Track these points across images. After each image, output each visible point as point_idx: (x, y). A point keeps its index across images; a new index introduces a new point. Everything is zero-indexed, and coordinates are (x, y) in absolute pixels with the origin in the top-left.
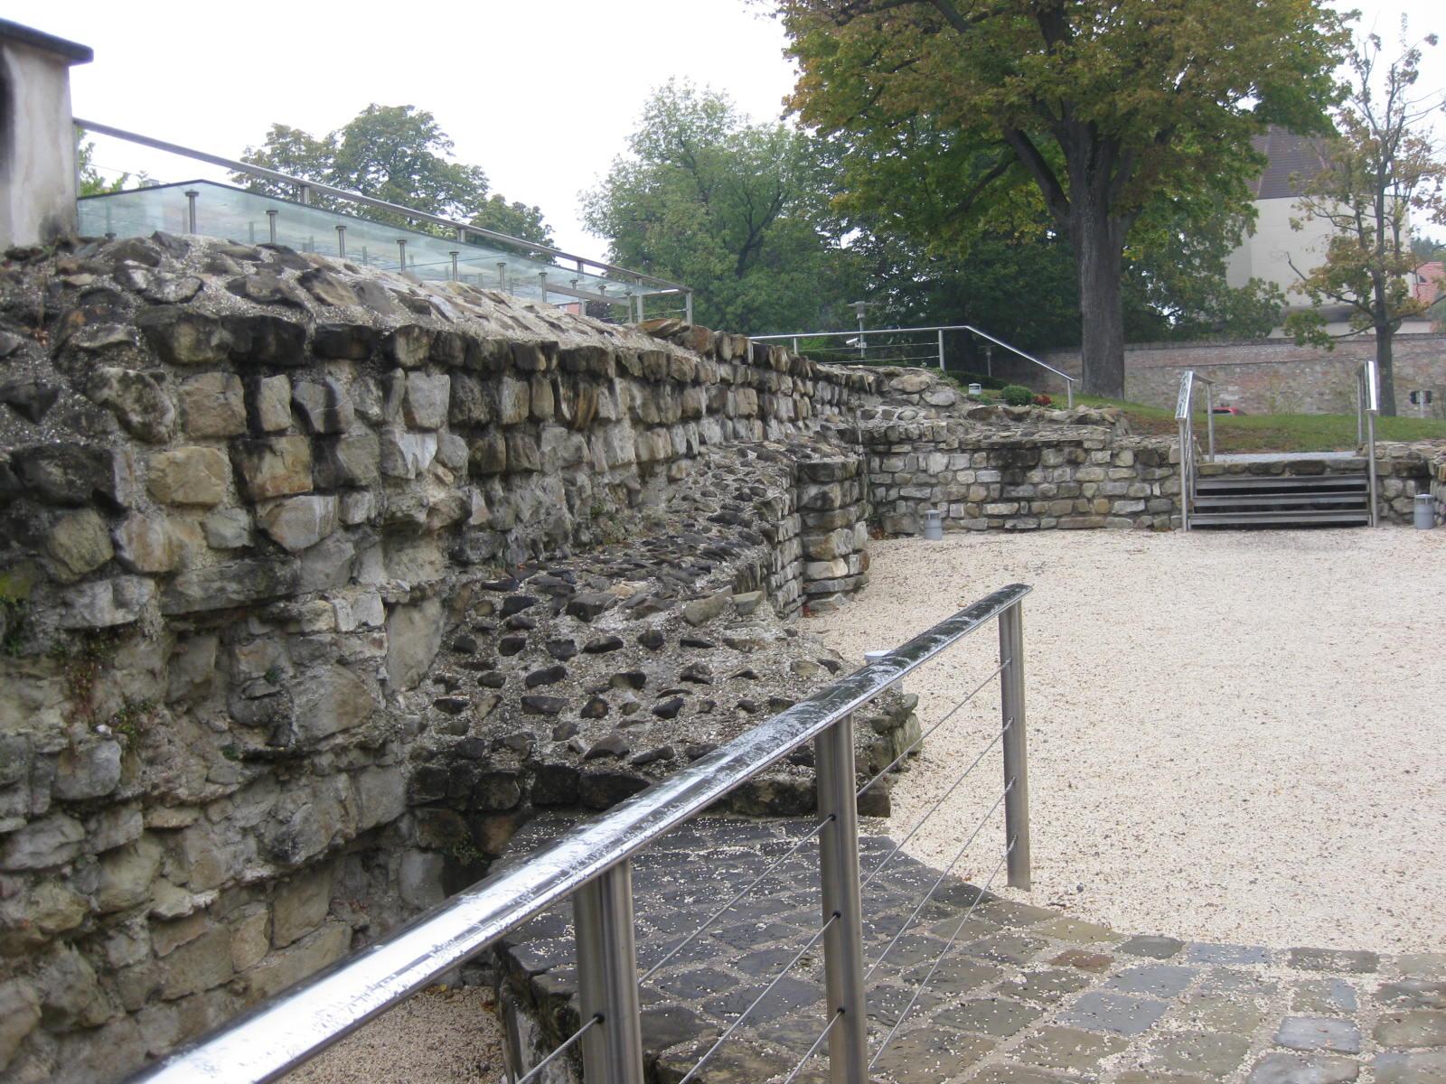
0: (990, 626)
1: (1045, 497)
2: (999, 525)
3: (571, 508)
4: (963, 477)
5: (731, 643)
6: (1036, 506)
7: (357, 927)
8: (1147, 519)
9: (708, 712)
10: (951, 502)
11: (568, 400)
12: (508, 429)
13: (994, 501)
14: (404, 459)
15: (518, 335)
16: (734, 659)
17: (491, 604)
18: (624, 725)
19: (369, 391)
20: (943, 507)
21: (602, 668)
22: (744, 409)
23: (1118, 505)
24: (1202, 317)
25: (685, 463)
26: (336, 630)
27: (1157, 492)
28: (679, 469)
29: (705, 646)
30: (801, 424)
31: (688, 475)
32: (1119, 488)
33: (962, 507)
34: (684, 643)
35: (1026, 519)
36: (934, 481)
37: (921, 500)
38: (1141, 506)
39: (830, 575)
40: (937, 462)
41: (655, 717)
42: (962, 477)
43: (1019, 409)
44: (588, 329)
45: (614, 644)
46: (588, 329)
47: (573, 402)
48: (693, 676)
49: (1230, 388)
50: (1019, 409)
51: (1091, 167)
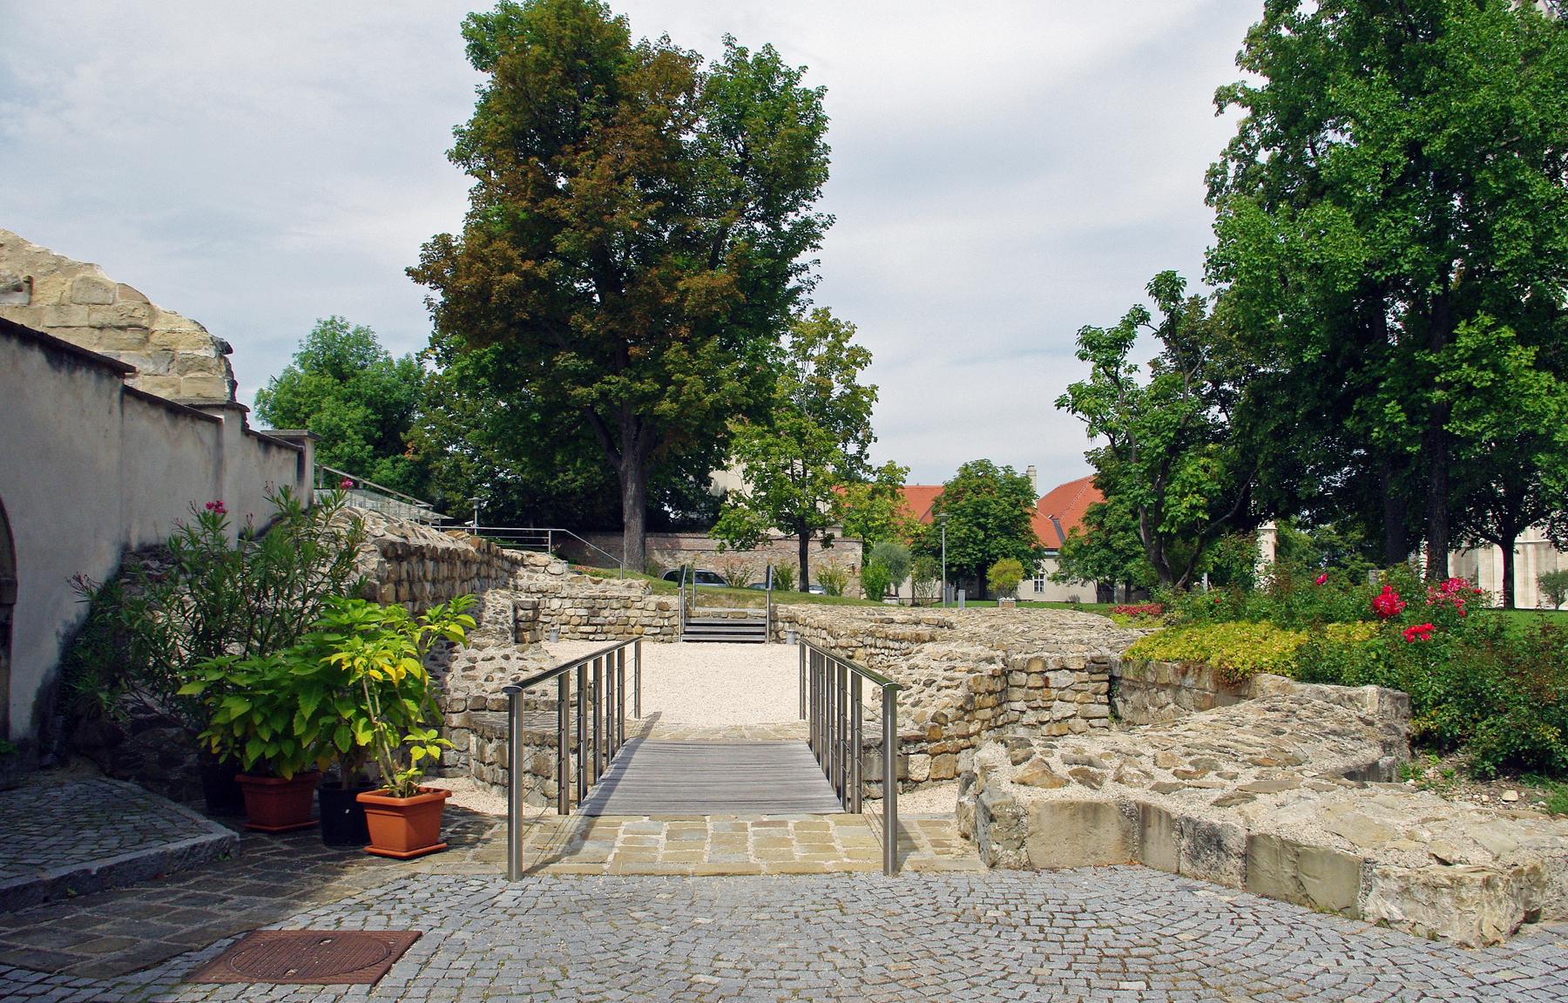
4: (570, 612)
8: (661, 637)
21: (489, 666)
24: (694, 516)
32: (646, 621)
38: (658, 630)
40: (555, 603)
42: (567, 611)
43: (596, 579)
45: (492, 658)
50: (596, 579)
51: (636, 439)
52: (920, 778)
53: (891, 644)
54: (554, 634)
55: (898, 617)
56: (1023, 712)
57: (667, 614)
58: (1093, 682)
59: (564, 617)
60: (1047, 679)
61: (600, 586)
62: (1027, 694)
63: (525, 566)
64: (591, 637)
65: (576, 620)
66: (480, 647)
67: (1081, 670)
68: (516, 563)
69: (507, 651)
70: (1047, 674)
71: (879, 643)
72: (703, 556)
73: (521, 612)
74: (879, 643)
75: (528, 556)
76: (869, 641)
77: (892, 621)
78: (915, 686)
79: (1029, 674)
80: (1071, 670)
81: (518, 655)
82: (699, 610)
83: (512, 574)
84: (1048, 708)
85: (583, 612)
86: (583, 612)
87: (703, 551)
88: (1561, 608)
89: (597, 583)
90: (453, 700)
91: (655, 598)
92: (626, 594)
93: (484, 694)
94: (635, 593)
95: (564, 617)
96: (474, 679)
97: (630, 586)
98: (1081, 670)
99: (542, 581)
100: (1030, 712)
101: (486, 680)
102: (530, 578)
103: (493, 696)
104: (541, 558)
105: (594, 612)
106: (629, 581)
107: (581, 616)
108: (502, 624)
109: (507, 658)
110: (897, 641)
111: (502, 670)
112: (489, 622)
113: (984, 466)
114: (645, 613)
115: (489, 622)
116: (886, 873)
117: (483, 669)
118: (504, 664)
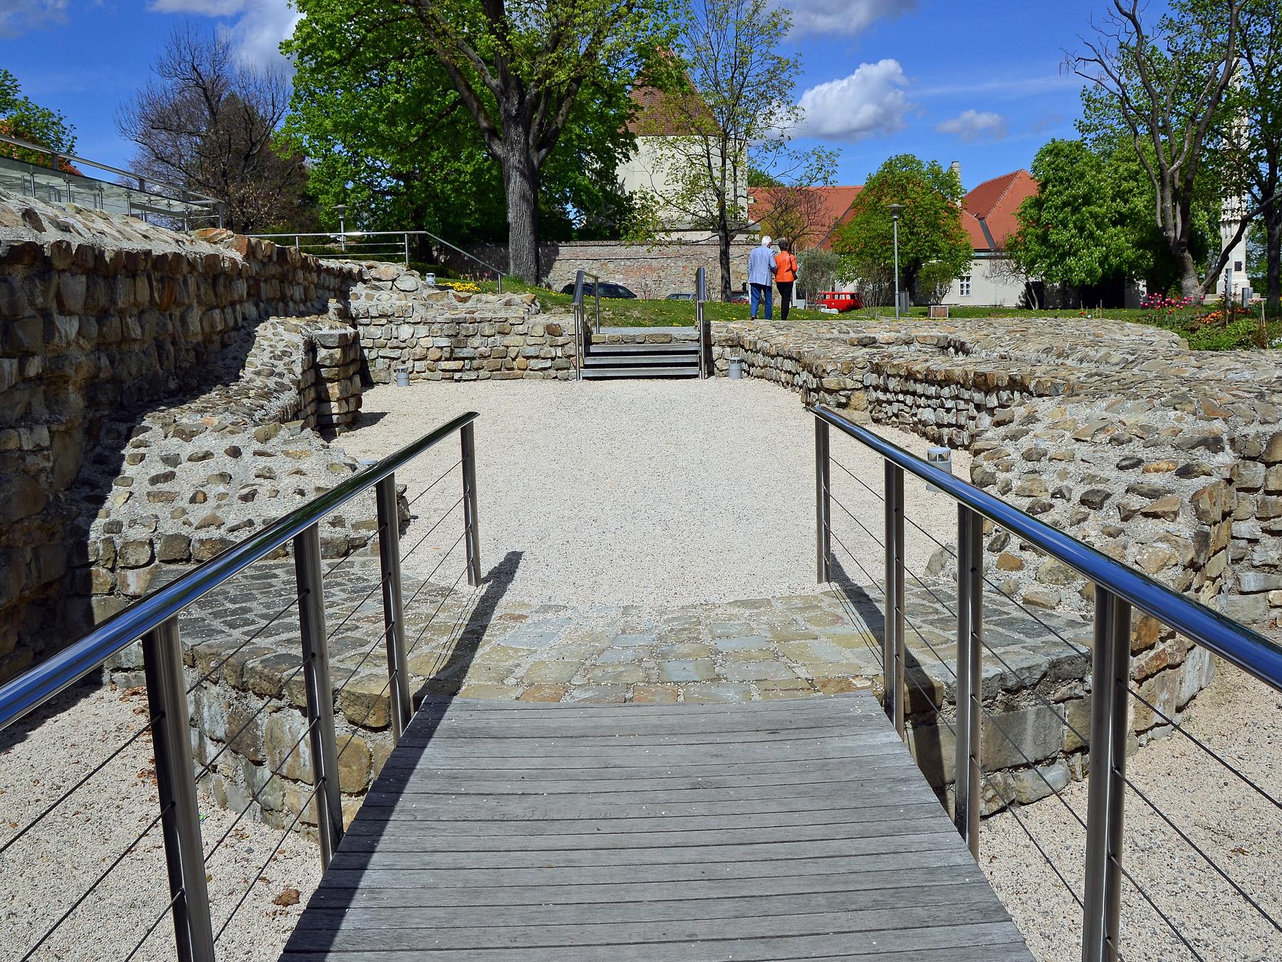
0: (456, 435)
1: (483, 357)
2: (449, 375)
3: (161, 365)
4: (426, 342)
5: (287, 454)
6: (476, 363)
7: (37, 650)
8: (553, 373)
9: (275, 496)
10: (414, 360)
11: (159, 290)
12: (121, 313)
13: (447, 359)
14: (60, 333)
15: (127, 246)
16: (290, 465)
17: (119, 432)
18: (219, 506)
19: (36, 286)
20: (409, 364)
21: (201, 471)
22: (271, 295)
23: (532, 362)
25: (233, 334)
26: (20, 449)
27: (560, 354)
28: (229, 337)
29: (270, 455)
30: (309, 304)
31: (235, 342)
32: (531, 351)
33: (424, 363)
34: (255, 453)
35: (469, 373)
36: (403, 345)
37: (394, 359)
38: (549, 363)
39: (993, 262)
40: (406, 332)
41: (239, 501)
44: (168, 239)
45: (206, 456)
46: (168, 239)
47: (161, 291)
48: (268, 475)
49: (617, 277)
53: (919, 388)
54: (403, 375)
56: (1254, 541)
57: (560, 340)
59: (418, 350)
61: (468, 304)
62: (1263, 505)
63: (365, 282)
64: (457, 376)
65: (434, 354)
66: (187, 435)
68: (349, 278)
69: (237, 440)
71: (893, 384)
72: (611, 266)
73: (322, 353)
74: (893, 384)
75: (370, 268)
76: (872, 379)
78: (1058, 502)
79: (1269, 465)
81: (257, 446)
82: (607, 332)
83: (343, 296)
85: (444, 342)
86: (444, 342)
87: (611, 260)
89: (464, 300)
90: (126, 545)
91: (543, 319)
92: (502, 314)
93: (185, 531)
94: (513, 314)
95: (418, 350)
96: (169, 498)
97: (508, 304)
99: (387, 300)
101: (193, 500)
102: (369, 297)
103: (203, 534)
104: (386, 269)
105: (458, 340)
106: (508, 296)
107: (441, 348)
108: (281, 375)
109: (235, 452)
110: (932, 383)
111: (225, 477)
112: (258, 373)
113: (907, 161)
114: (530, 340)
115: (258, 373)
116: (820, 581)
117: (189, 476)
118: (229, 465)
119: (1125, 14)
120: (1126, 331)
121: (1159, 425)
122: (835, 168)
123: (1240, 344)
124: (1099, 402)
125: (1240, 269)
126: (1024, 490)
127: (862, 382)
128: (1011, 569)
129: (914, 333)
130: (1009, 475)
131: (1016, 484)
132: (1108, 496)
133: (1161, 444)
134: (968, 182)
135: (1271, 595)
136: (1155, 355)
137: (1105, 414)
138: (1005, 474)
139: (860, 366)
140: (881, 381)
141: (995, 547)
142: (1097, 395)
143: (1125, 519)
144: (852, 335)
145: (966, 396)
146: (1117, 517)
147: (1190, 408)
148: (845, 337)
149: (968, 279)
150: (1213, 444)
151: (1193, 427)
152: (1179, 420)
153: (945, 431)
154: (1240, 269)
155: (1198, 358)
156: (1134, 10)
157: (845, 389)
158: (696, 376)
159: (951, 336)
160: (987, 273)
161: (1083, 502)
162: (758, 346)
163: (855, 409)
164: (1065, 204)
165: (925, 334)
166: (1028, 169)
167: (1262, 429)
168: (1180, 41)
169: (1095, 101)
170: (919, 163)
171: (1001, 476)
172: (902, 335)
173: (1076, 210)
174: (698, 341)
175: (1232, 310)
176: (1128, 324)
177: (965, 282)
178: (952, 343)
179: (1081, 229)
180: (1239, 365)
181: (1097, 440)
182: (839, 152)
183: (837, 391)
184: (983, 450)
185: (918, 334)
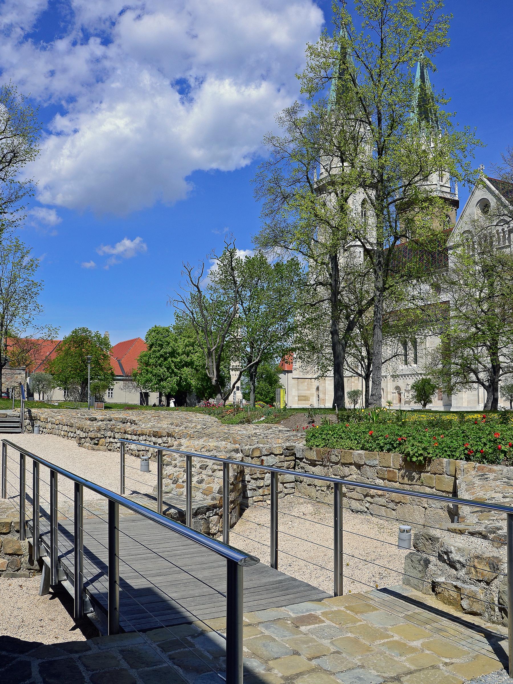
52: (215, 532)
53: (129, 437)
55: (99, 417)
58: (287, 461)
60: (262, 460)
67: (281, 455)
70: (263, 458)
76: (109, 434)
77: (95, 419)
79: (252, 458)
80: (276, 455)
84: (263, 479)
88: (428, 407)
98: (281, 455)
100: (253, 481)
110: (135, 435)
113: (84, 330)
119: (195, 285)
120: (198, 417)
121: (220, 446)
122: (57, 335)
123: (241, 422)
124: (201, 440)
125: (239, 390)
126: (181, 466)
127: (104, 435)
128: (180, 488)
129: (112, 416)
130: (176, 462)
131: (178, 464)
132: (208, 466)
133: (222, 451)
134: (113, 343)
135: (254, 498)
136: (213, 426)
137: (203, 443)
138: (174, 462)
139: (103, 429)
140: (112, 435)
141: (174, 482)
142: (199, 438)
143: (213, 472)
144: (86, 416)
145: (150, 440)
146: (211, 472)
147: (230, 441)
148: (84, 417)
149: (112, 390)
150: (237, 451)
151: (230, 446)
152: (226, 444)
153: (141, 452)
154: (239, 390)
155: (228, 427)
156: (198, 284)
157: (97, 438)
158: (19, 433)
159: (128, 418)
160: (122, 387)
161: (200, 468)
162: (49, 420)
163: (101, 446)
164: (161, 356)
165: (117, 417)
166: (144, 339)
167: (249, 447)
168: (215, 295)
169: (180, 317)
170: (90, 332)
171: (173, 462)
172: (107, 417)
173: (166, 359)
174: (19, 417)
175: (236, 408)
176: (198, 414)
177: (111, 391)
178: (129, 421)
179: (168, 369)
180: (242, 429)
181: (202, 450)
182: (60, 328)
183: (94, 439)
184: (166, 455)
185: (114, 417)
